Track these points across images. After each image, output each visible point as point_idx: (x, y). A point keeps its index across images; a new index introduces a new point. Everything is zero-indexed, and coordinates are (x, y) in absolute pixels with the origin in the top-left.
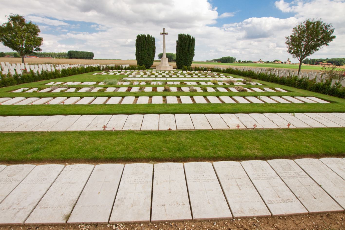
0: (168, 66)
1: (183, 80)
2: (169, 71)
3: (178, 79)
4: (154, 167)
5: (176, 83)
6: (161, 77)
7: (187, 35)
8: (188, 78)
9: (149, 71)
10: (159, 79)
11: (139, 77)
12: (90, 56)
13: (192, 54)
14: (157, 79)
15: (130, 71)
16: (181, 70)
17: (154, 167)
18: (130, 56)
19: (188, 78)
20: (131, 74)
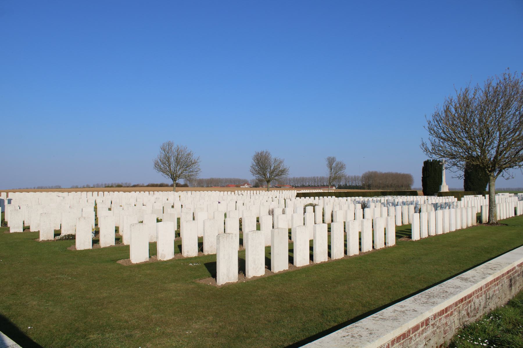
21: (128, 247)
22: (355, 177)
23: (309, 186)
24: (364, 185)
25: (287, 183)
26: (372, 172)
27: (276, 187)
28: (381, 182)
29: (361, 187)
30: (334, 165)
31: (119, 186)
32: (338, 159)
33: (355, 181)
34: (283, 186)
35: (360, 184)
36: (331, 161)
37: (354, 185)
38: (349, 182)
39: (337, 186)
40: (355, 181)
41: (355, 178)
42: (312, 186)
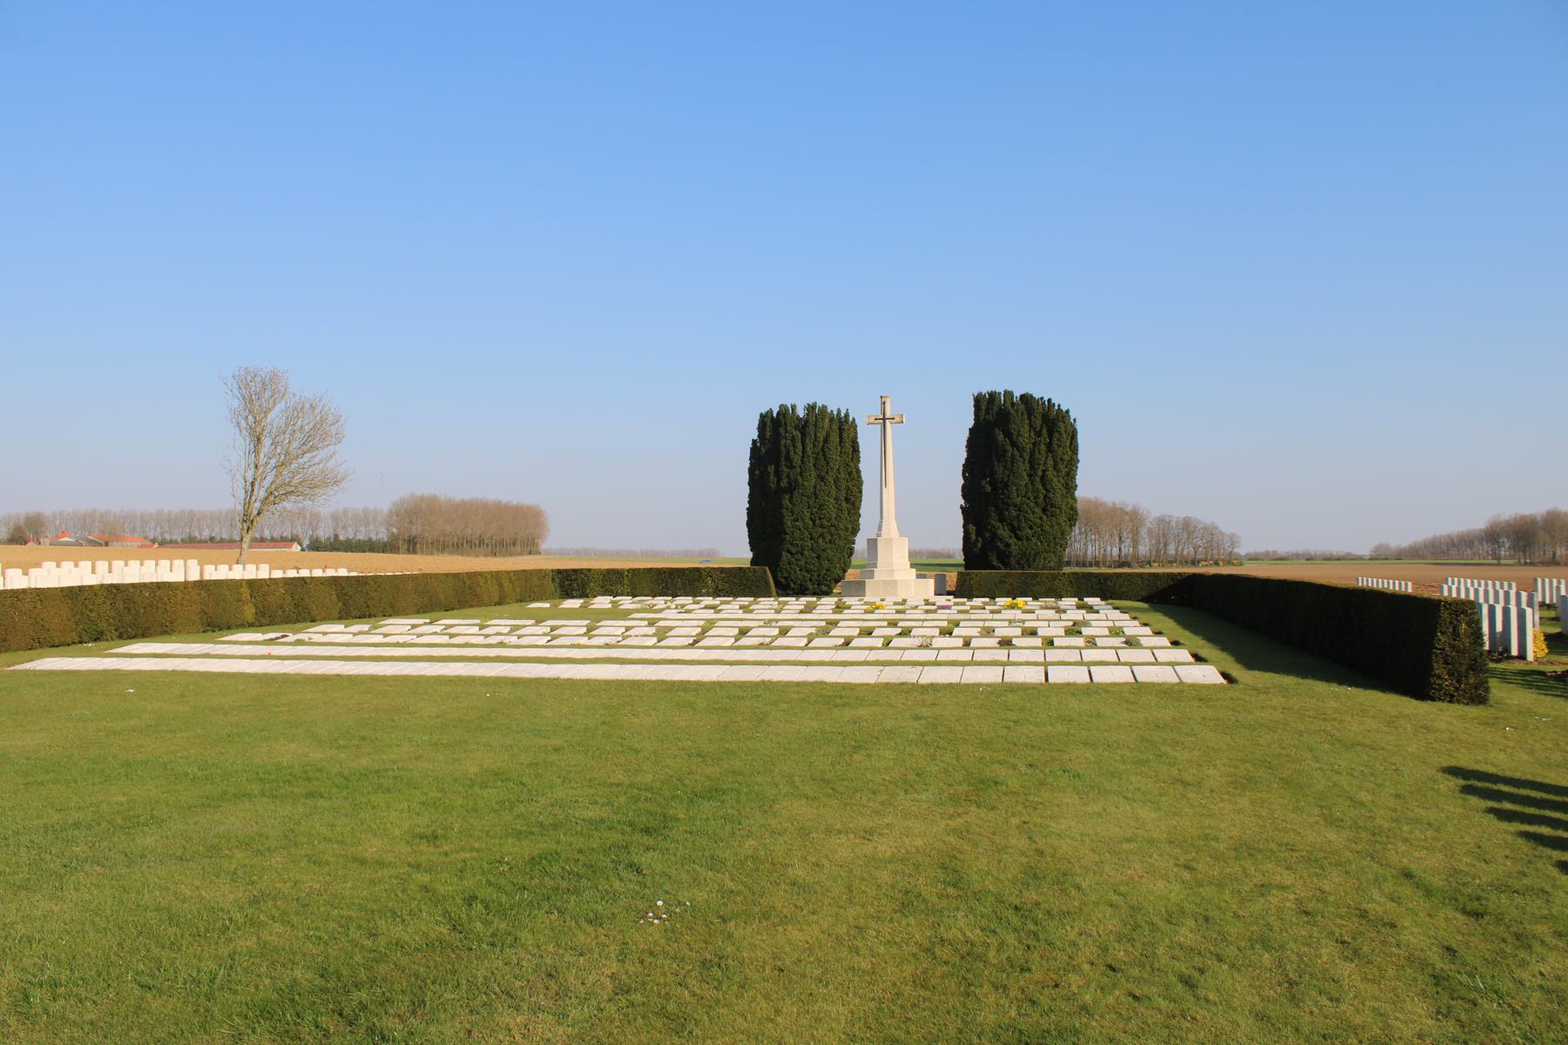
21: (811, 408)
22: (366, 512)
23: (212, 539)
24: (395, 538)
25: (134, 530)
26: (422, 498)
27: (93, 543)
28: (448, 529)
29: (385, 545)
30: (275, 417)
31: (1282, 559)
32: (301, 386)
33: (367, 525)
34: (118, 539)
35: (382, 535)
36: (255, 399)
37: (361, 537)
38: (344, 527)
39: (306, 543)
40: (367, 525)
41: (367, 517)
42: (222, 541)
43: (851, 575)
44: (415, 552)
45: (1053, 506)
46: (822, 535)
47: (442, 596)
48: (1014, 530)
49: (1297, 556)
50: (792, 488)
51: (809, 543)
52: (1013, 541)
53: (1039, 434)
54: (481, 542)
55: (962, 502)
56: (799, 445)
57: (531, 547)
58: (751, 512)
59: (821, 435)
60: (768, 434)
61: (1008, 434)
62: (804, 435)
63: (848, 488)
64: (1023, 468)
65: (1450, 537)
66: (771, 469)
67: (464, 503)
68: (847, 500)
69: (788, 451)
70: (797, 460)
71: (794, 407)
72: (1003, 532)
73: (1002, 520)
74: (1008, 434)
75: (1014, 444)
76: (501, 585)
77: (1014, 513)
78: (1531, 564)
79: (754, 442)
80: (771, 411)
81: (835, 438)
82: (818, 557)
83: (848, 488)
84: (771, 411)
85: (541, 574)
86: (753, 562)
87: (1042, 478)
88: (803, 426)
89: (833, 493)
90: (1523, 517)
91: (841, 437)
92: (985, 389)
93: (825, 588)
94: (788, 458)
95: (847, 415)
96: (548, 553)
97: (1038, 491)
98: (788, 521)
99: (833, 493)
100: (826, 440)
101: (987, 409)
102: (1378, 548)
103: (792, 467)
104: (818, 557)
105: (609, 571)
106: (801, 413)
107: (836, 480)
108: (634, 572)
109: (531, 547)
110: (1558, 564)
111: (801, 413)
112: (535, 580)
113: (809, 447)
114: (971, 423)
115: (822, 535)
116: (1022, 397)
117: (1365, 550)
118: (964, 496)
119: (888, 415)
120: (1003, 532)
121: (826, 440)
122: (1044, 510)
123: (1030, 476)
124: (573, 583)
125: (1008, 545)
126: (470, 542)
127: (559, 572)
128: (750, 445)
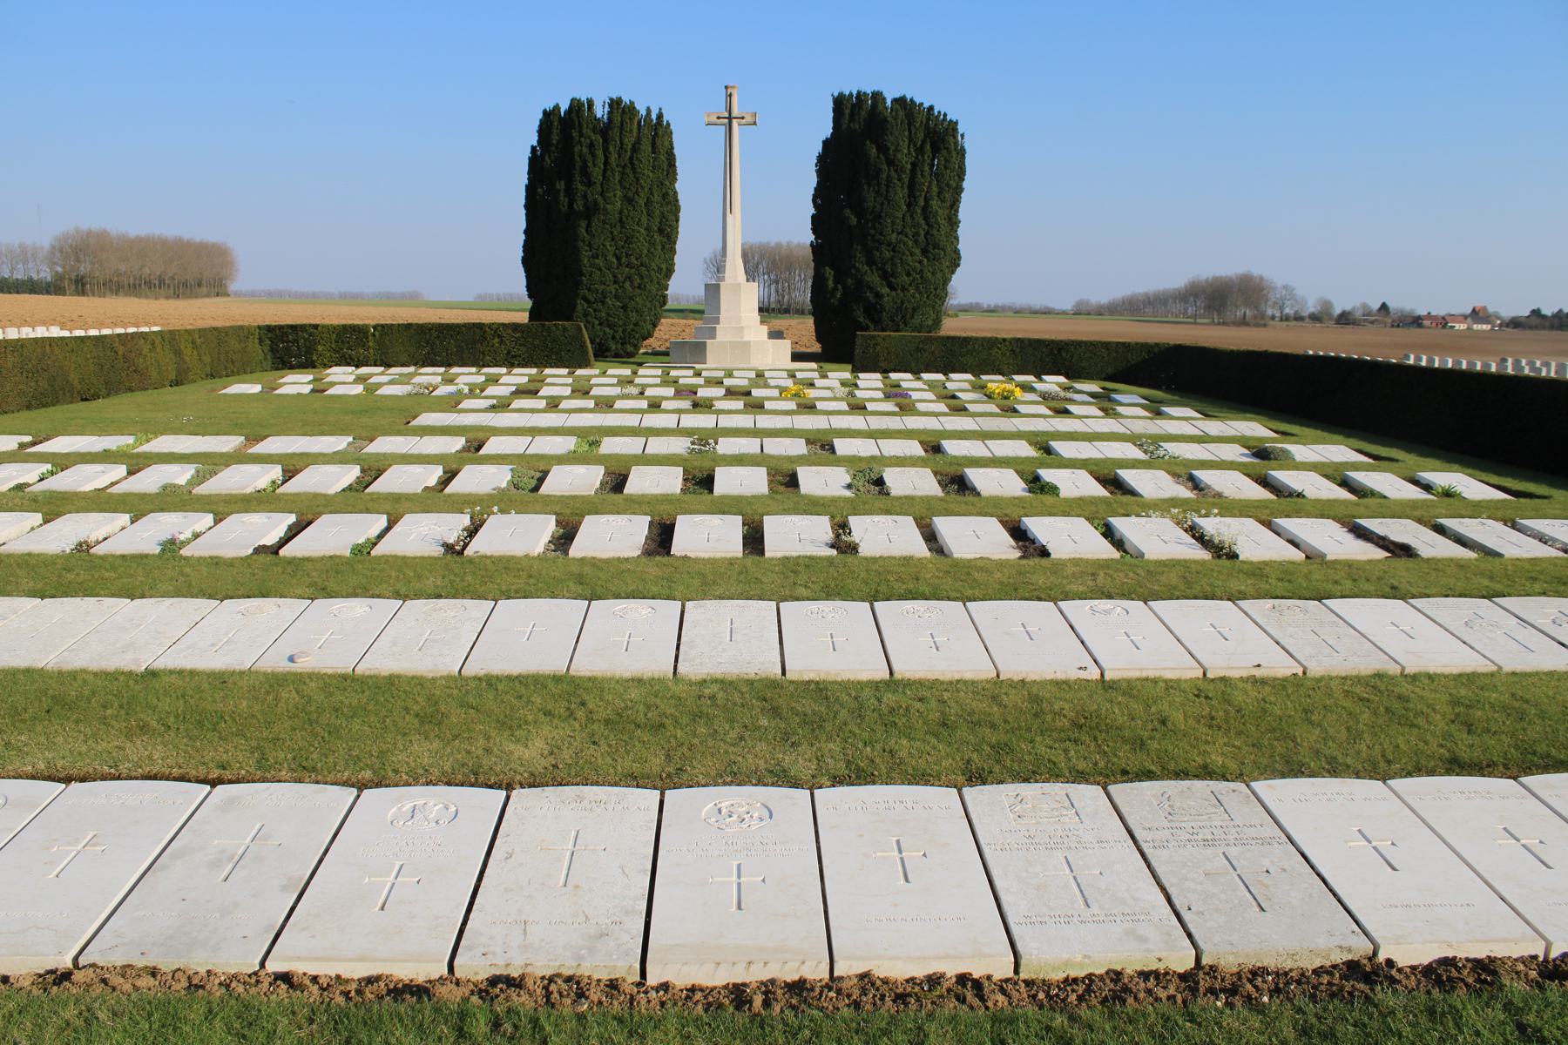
0: (750, 339)
1: (1106, 460)
2: (760, 375)
3: (912, 422)
4: (662, 803)
5: (776, 447)
6: (679, 411)
7: (900, 101)
8: (982, 415)
9: (610, 372)
10: (668, 421)
11: (542, 416)
12: (198, 270)
13: (940, 252)
14: (653, 420)
15: (478, 373)
16: (850, 367)
17: (662, 803)
18: (487, 273)
19: (982, 415)
20: (475, 391)
24: (60, 278)
26: (89, 233)
28: (122, 268)
29: (48, 285)
31: (1036, 313)
33: (25, 262)
35: (46, 275)
37: (19, 275)
40: (25, 262)
41: (25, 254)
43: (667, 331)
44: (83, 293)
45: (936, 246)
46: (629, 278)
47: (74, 377)
48: (885, 276)
49: (270, 294)
50: (590, 211)
51: (612, 288)
52: (885, 290)
53: (920, 151)
54: (162, 283)
55: (812, 237)
56: (600, 153)
57: (217, 287)
58: (527, 247)
59: (629, 141)
60: (555, 138)
61: (883, 149)
62: (606, 141)
63: (663, 215)
64: (901, 194)
65: (1147, 295)
66: (561, 185)
67: (139, 241)
68: (661, 231)
69: (585, 162)
70: (596, 173)
71: (590, 103)
72: (874, 278)
73: (870, 262)
74: (883, 149)
75: (891, 162)
76: (178, 353)
77: (888, 254)
78: (1225, 324)
79: (533, 149)
80: (557, 107)
81: (646, 146)
82: (624, 307)
83: (663, 215)
84: (557, 107)
85: (241, 332)
86: (534, 314)
87: (924, 209)
88: (605, 129)
89: (644, 220)
90: (1216, 279)
91: (654, 145)
92: (850, 88)
93: (630, 349)
94: (585, 172)
95: (660, 116)
96: (238, 294)
97: (918, 225)
98: (585, 256)
99: (644, 220)
100: (635, 149)
101: (852, 115)
102: (1079, 303)
103: (590, 184)
104: (624, 307)
105: (345, 328)
106: (600, 111)
107: (648, 203)
108: (384, 330)
109: (217, 287)
110: (1247, 324)
111: (600, 111)
112: (234, 343)
113: (614, 158)
114: (827, 131)
115: (629, 278)
116: (895, 101)
117: (1068, 305)
118: (814, 230)
119: (735, 113)
120: (874, 278)
121: (635, 149)
122: (925, 252)
123: (909, 205)
124: (291, 346)
125: (878, 296)
126: (149, 284)
127: (270, 329)
128: (528, 153)
